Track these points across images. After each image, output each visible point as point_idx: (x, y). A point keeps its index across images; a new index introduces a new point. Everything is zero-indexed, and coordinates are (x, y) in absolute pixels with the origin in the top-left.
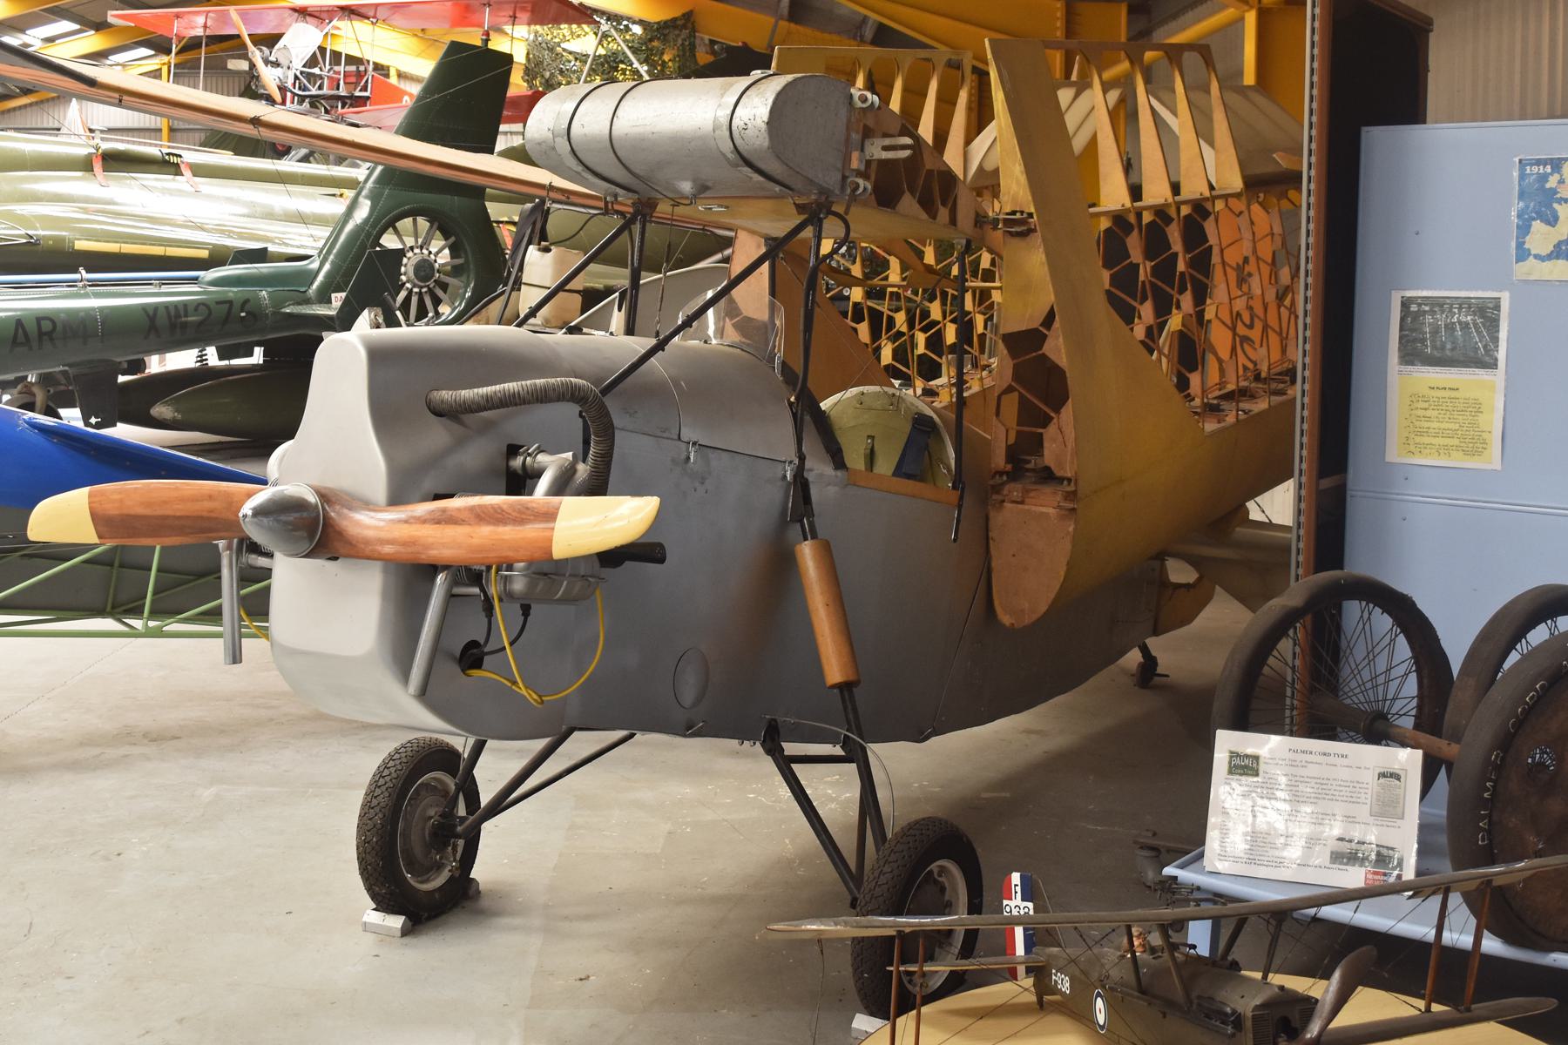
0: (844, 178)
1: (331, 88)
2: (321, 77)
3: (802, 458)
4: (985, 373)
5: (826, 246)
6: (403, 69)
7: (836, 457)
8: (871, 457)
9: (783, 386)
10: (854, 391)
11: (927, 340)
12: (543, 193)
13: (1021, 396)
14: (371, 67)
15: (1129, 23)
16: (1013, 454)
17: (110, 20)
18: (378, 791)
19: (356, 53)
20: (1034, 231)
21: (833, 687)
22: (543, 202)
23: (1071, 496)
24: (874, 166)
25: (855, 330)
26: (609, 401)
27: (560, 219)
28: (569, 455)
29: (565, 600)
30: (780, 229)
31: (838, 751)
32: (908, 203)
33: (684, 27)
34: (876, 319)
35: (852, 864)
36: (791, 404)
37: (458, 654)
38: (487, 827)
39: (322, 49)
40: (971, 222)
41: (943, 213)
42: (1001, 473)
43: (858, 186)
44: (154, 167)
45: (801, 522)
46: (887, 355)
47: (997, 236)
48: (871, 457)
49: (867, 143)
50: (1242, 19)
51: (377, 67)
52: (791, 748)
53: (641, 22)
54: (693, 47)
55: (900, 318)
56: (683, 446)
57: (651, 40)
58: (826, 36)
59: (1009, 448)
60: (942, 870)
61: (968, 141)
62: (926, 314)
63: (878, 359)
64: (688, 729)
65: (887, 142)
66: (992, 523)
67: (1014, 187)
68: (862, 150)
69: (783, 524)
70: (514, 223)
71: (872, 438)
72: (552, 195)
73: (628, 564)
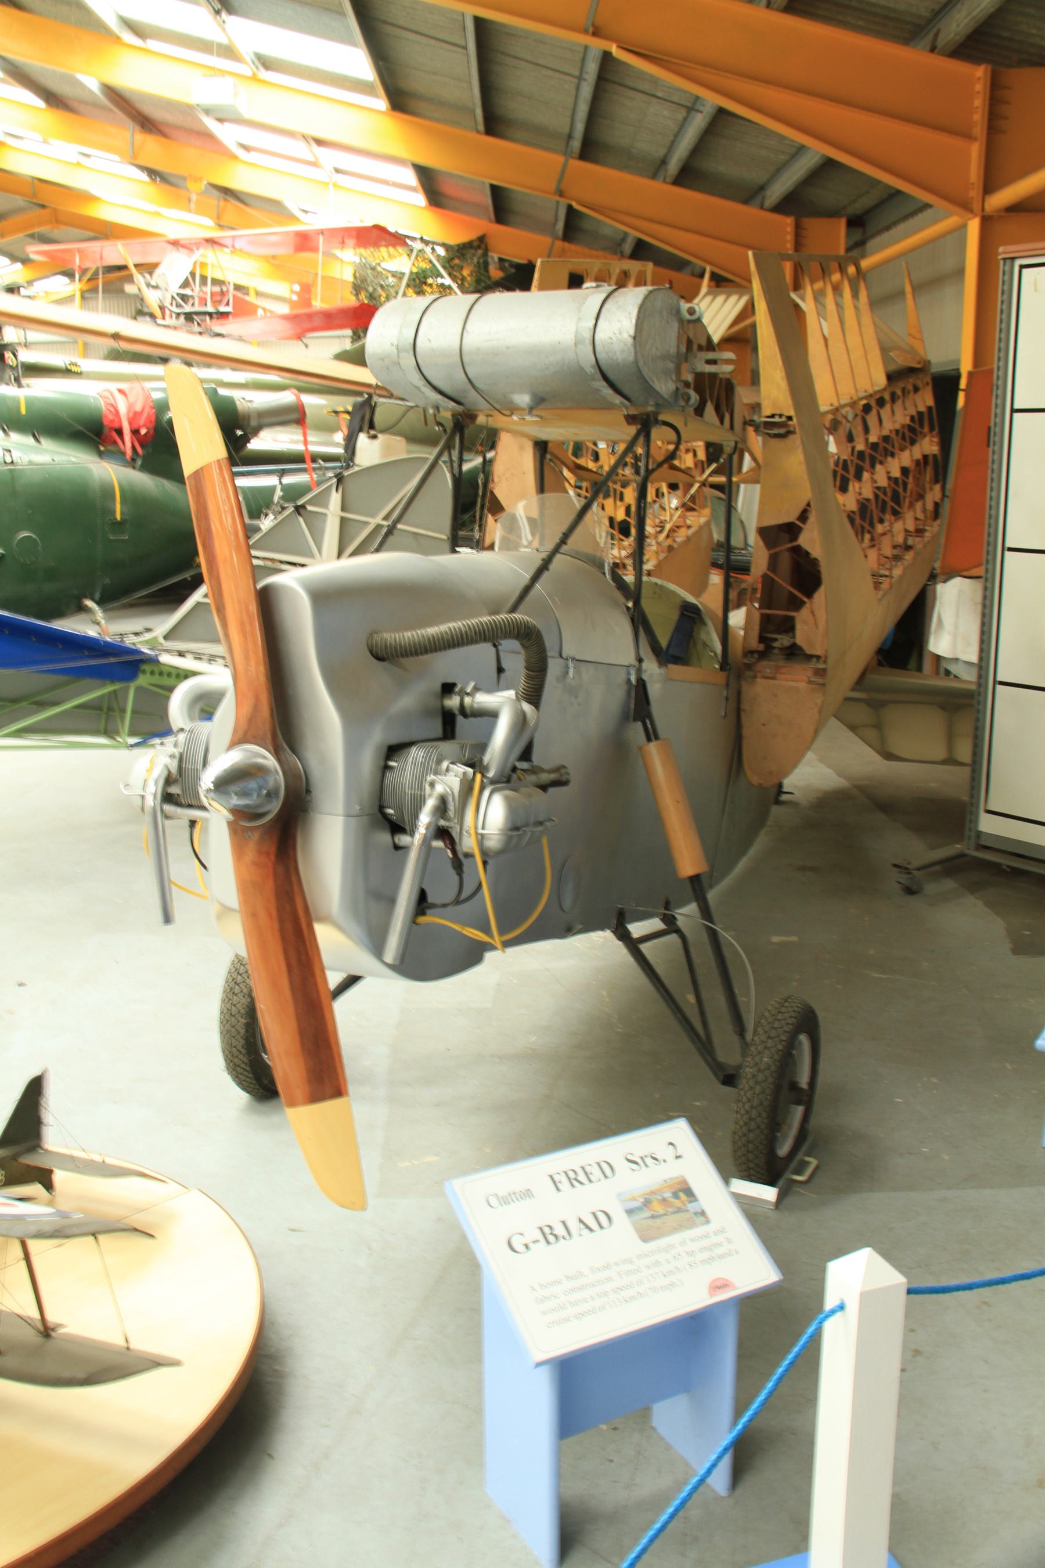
1: (200, 304)
2: (192, 297)
6: (261, 289)
12: (371, 391)
14: (231, 288)
15: (848, 235)
17: (33, 256)
19: (219, 276)
20: (793, 432)
22: (370, 396)
23: (821, 673)
27: (385, 409)
33: (479, 247)
39: (193, 274)
41: (867, 537)
42: (752, 652)
44: (60, 375)
50: (964, 226)
51: (237, 288)
53: (443, 245)
54: (486, 264)
57: (452, 259)
58: (594, 252)
65: (711, 355)
66: (744, 696)
70: (348, 412)
72: (378, 392)
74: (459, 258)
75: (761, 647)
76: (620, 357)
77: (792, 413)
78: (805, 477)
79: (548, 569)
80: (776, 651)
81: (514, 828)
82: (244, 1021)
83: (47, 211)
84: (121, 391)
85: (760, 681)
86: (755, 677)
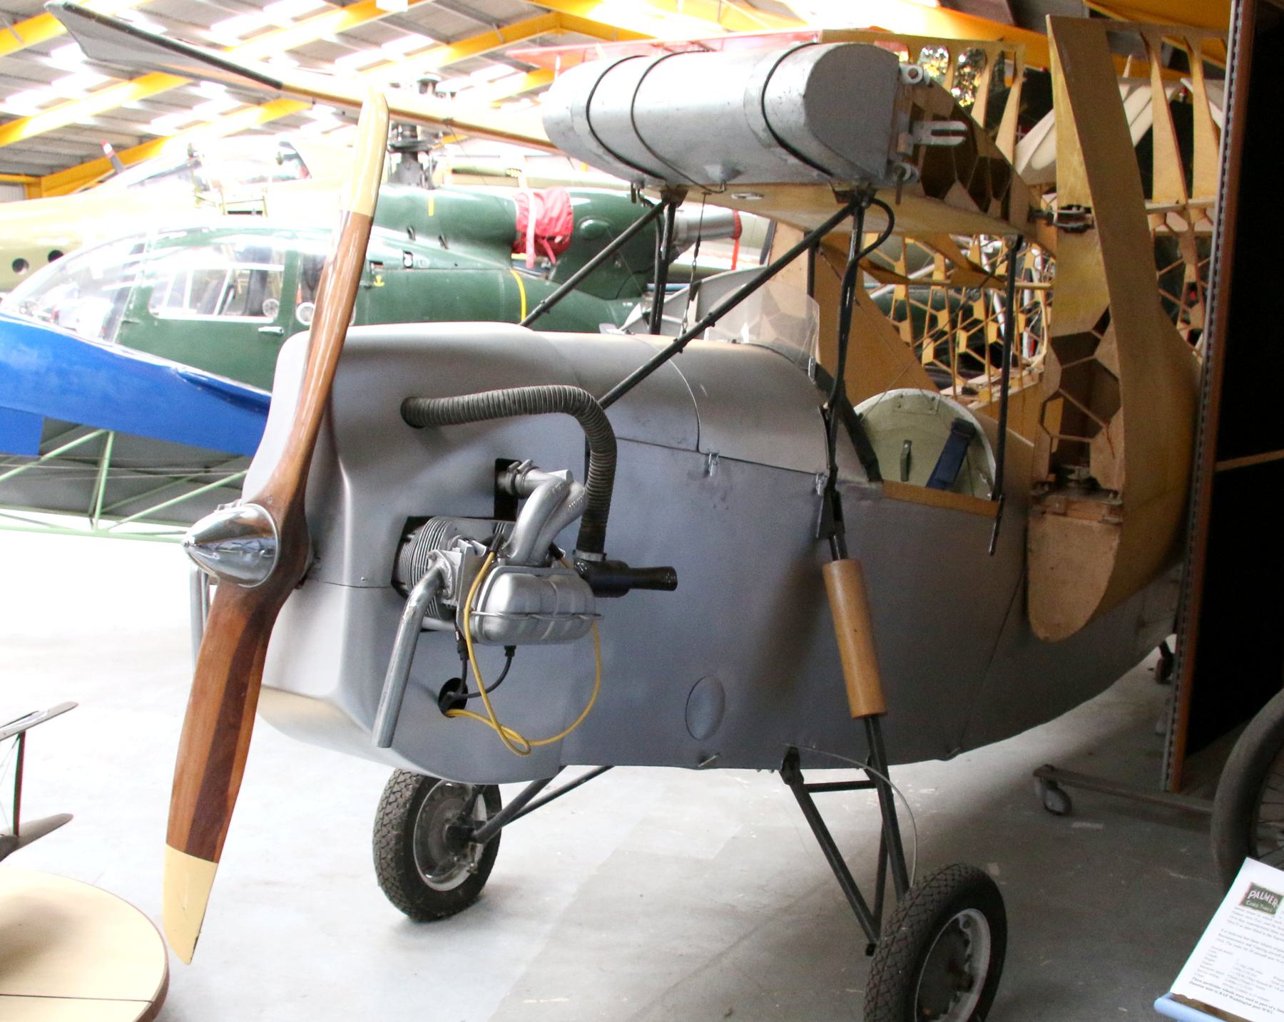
0: (889, 162)
3: (834, 470)
4: (1025, 373)
5: (869, 239)
7: (870, 466)
8: (907, 463)
9: (817, 392)
10: (893, 393)
11: (970, 339)
13: (1066, 401)
16: (1057, 465)
18: (389, 809)
20: (1091, 227)
21: (860, 718)
24: (923, 151)
25: (897, 329)
26: (611, 414)
28: (562, 474)
29: (557, 638)
30: (816, 221)
31: (859, 775)
32: (958, 193)
34: (918, 317)
35: (871, 908)
36: (824, 411)
37: (438, 691)
38: (508, 831)
40: (1024, 217)
41: (995, 206)
42: (1043, 484)
43: (903, 172)
45: (831, 539)
46: (928, 354)
47: (1050, 233)
48: (907, 463)
49: (916, 127)
52: (811, 776)
55: (943, 318)
56: (703, 459)
59: (1053, 456)
60: (969, 922)
61: (1017, 140)
62: (968, 311)
63: (920, 358)
64: (701, 761)
65: (939, 126)
66: (1030, 534)
67: (1072, 179)
68: (911, 131)
69: (814, 542)
71: (909, 442)
73: (632, 592)
74: (972, 67)
75: (1052, 478)
76: (794, 118)
77: (1090, 204)
78: (1104, 279)
79: (681, 351)
80: (1072, 485)
81: (515, 615)
82: (395, 832)
83: (551, 15)
84: (537, 195)
85: (1050, 518)
86: (1044, 513)
